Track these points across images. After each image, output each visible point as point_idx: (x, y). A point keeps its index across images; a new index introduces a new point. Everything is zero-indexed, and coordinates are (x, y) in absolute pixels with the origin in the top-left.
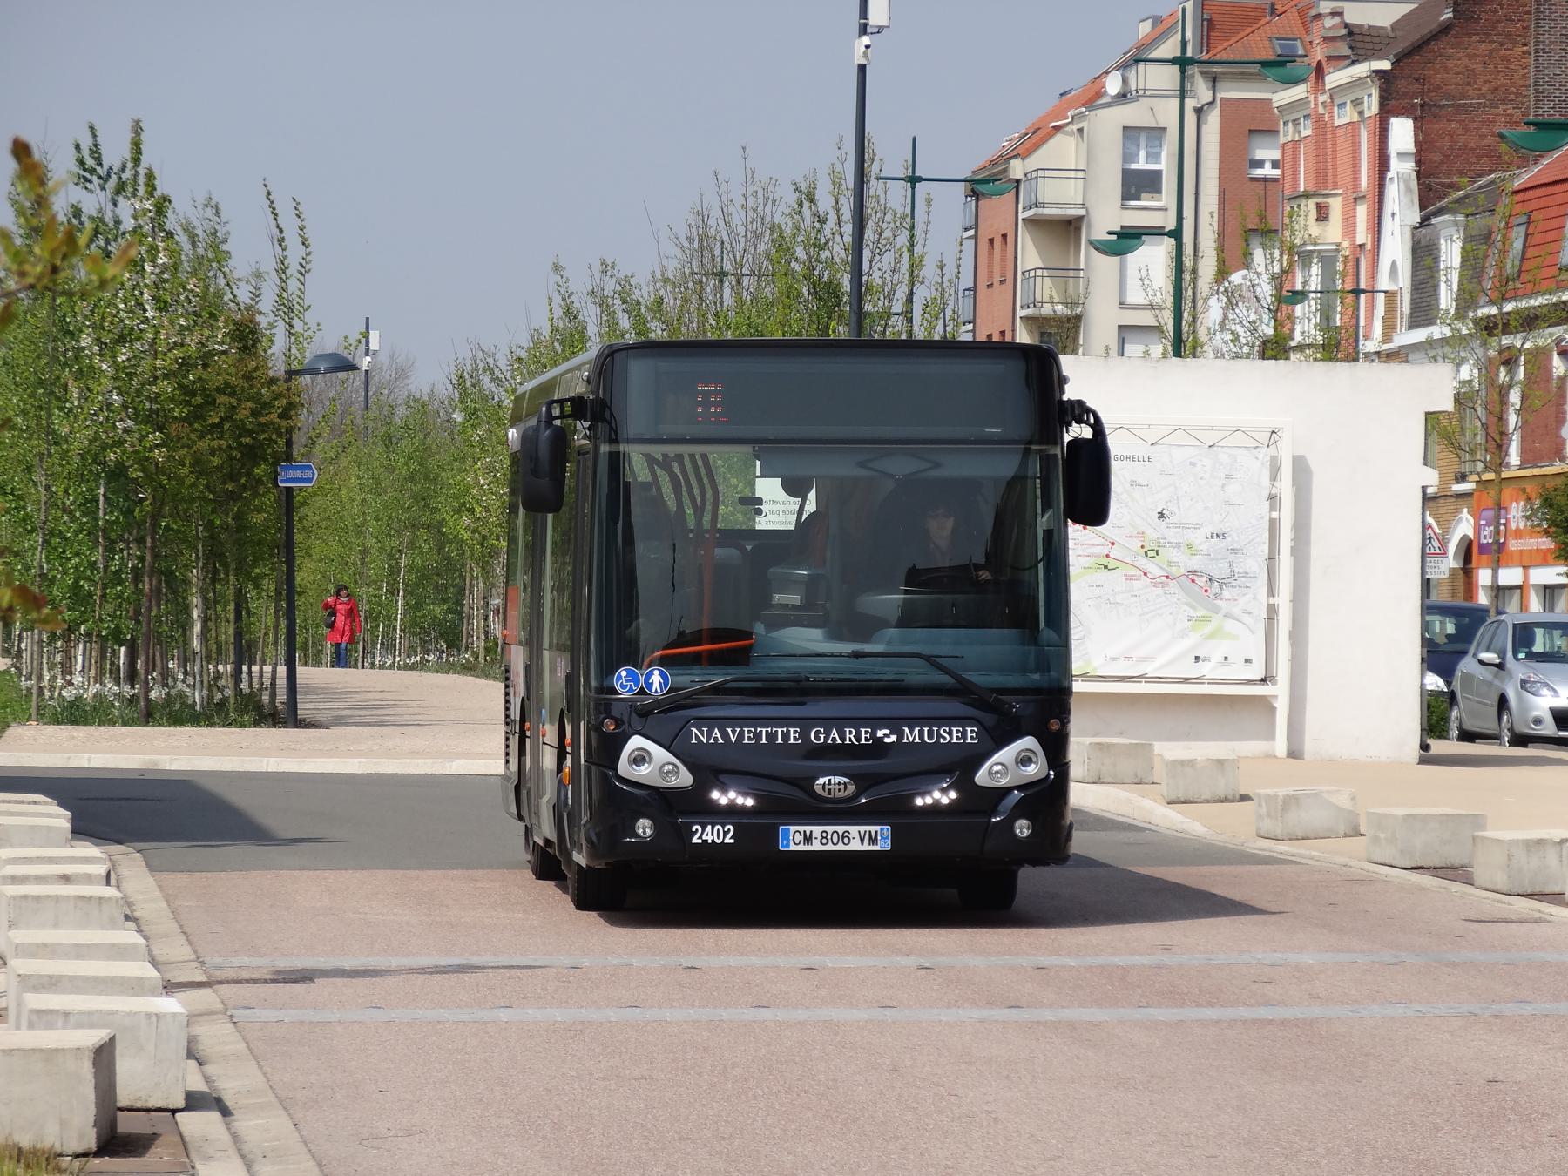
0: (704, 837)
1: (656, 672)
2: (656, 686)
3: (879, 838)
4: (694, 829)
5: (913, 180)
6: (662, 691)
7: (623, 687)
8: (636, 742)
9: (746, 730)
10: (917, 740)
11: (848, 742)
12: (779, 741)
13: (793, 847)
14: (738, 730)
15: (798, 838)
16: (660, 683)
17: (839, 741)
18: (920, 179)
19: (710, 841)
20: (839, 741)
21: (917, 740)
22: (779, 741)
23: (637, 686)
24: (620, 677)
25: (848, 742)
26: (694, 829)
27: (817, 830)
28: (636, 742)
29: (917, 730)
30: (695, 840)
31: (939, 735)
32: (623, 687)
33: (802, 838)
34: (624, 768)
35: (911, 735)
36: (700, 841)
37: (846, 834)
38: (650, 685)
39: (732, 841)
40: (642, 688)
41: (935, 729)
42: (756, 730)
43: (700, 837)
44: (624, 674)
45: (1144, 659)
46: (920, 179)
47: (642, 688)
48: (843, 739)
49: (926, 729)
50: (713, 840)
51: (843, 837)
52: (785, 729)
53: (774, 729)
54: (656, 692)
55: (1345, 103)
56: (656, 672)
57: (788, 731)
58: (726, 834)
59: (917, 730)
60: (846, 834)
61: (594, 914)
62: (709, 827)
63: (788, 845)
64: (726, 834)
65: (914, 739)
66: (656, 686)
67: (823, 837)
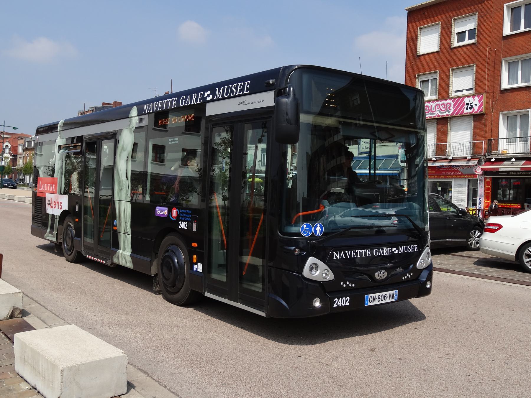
0: (338, 304)
1: (319, 225)
2: (318, 232)
3: (394, 296)
4: (335, 301)
5: (4, 126)
6: (320, 234)
7: (305, 233)
8: (311, 260)
9: (353, 251)
10: (403, 252)
11: (385, 254)
12: (364, 256)
13: (369, 304)
14: (350, 251)
15: (371, 299)
16: (320, 230)
17: (382, 254)
18: (5, 126)
19: (340, 305)
20: (382, 254)
21: (403, 252)
22: (364, 256)
23: (311, 232)
24: (303, 228)
25: (385, 254)
26: (335, 301)
27: (377, 295)
28: (311, 260)
29: (403, 247)
30: (335, 306)
31: (409, 249)
32: (305, 233)
33: (372, 299)
34: (306, 272)
35: (401, 250)
36: (337, 306)
37: (386, 296)
38: (316, 232)
39: (348, 304)
40: (313, 233)
41: (407, 246)
42: (356, 251)
43: (337, 304)
44: (305, 226)
45: (126, 184)
46: (5, 126)
47: (313, 233)
48: (383, 253)
49: (405, 247)
50: (341, 305)
51: (385, 297)
52: (365, 250)
53: (362, 250)
54: (318, 235)
55: (428, 81)
56: (319, 225)
57: (366, 251)
58: (346, 301)
59: (403, 247)
60: (386, 296)
61: (192, 309)
62: (341, 298)
63: (367, 304)
64: (346, 301)
65: (402, 251)
66: (318, 232)
67: (379, 298)
